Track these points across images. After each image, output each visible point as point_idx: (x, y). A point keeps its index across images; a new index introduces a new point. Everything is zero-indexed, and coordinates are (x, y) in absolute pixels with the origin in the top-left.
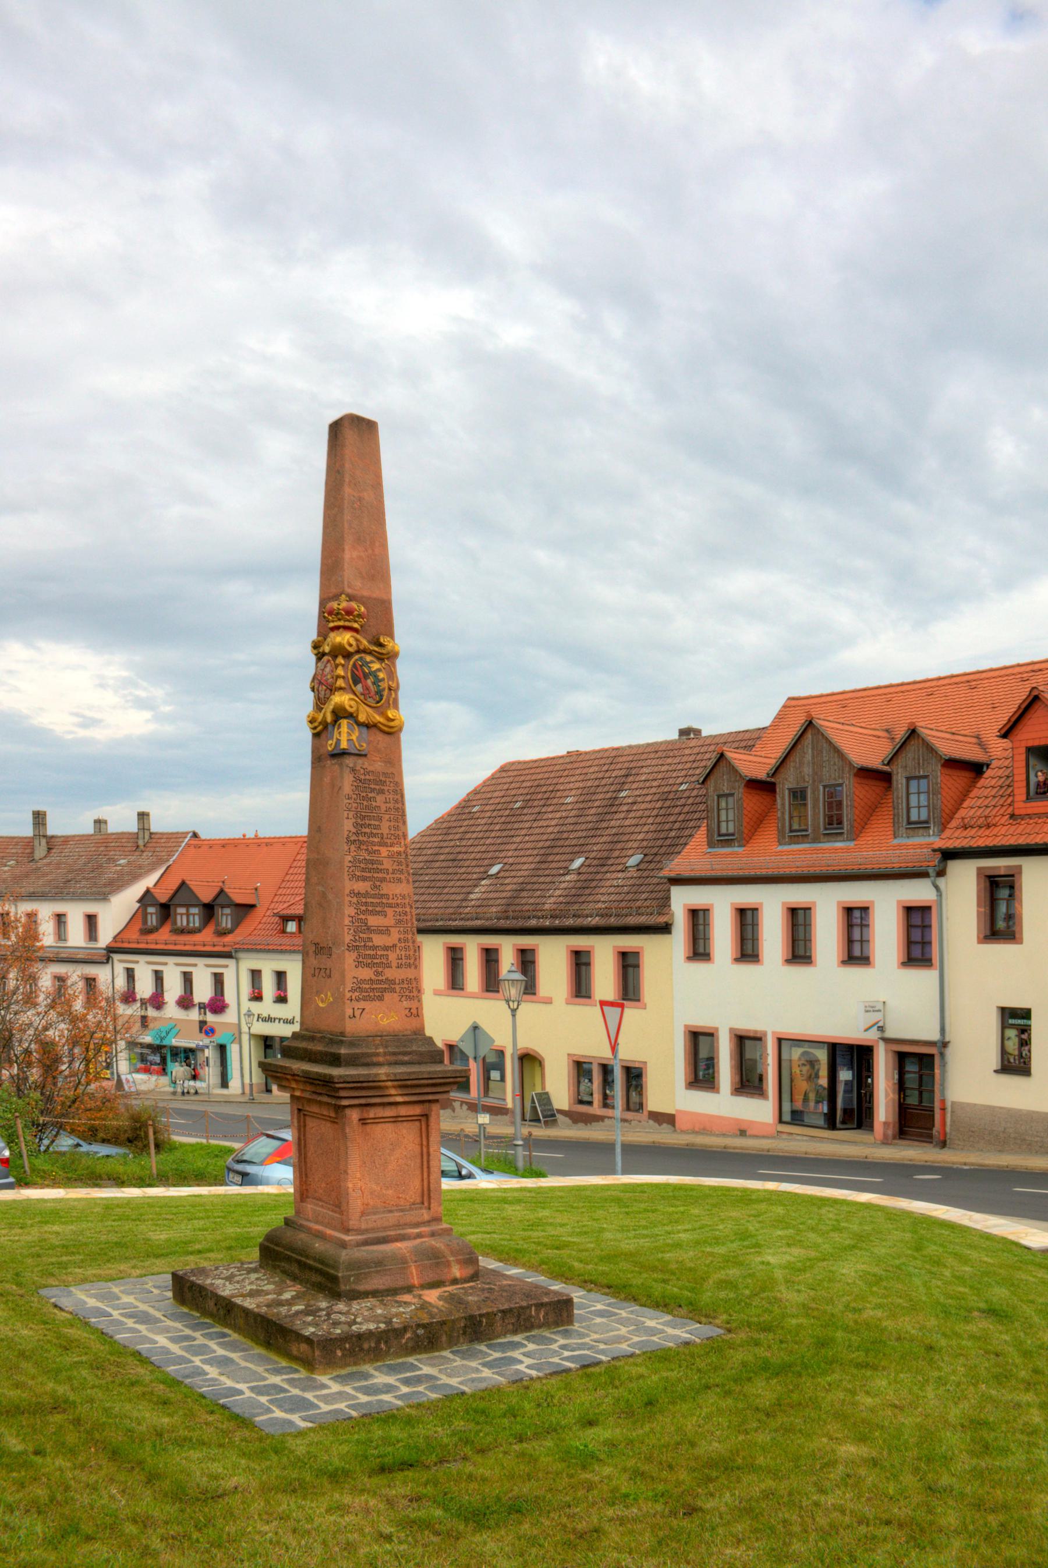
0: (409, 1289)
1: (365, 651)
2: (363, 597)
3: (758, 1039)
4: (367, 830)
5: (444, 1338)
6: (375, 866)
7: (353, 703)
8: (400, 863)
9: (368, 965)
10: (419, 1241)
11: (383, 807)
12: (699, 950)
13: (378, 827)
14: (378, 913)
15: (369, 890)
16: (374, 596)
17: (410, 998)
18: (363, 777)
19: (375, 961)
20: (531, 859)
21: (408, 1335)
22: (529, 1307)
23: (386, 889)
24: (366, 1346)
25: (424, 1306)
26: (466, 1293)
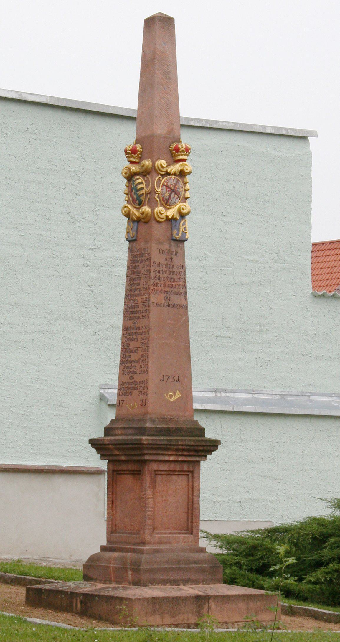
17: (143, 393)
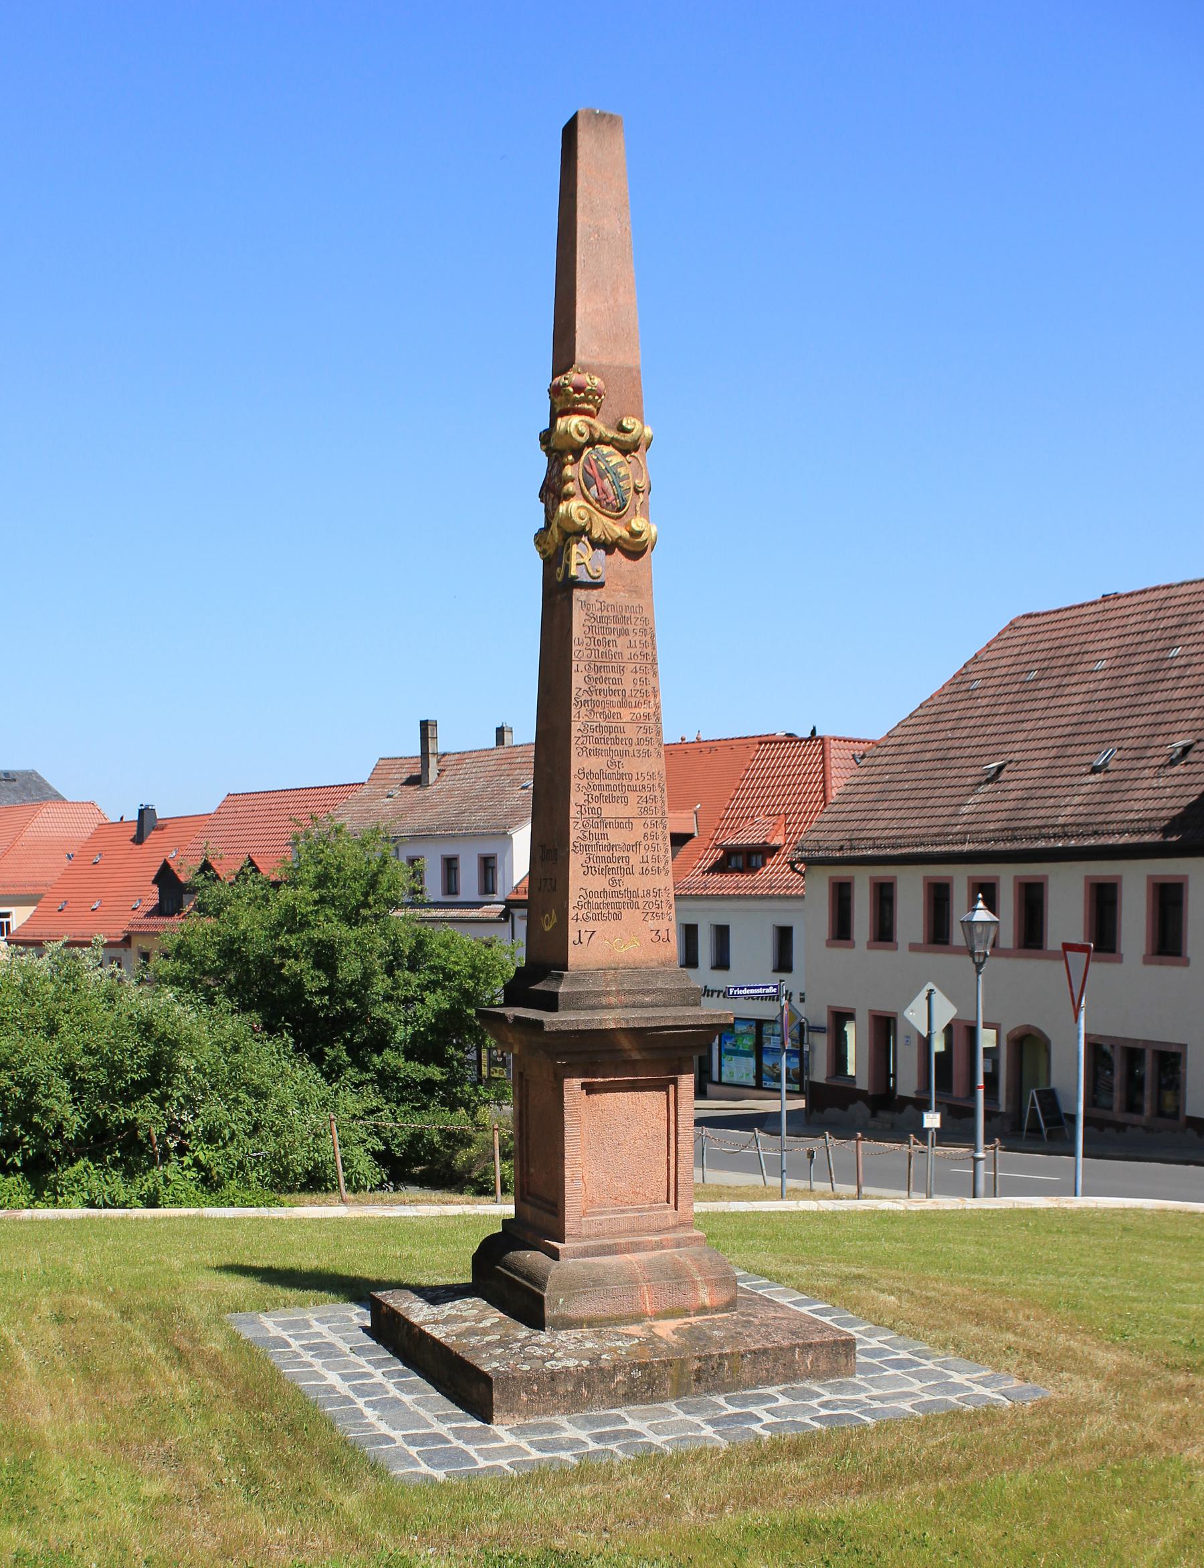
0: (637, 1319)
2: (601, 366)
4: (604, 686)
5: (669, 1384)
6: (613, 735)
7: (582, 512)
9: (600, 871)
10: (657, 1253)
14: (616, 800)
16: (617, 363)
18: (599, 614)
19: (611, 866)
20: (1044, 753)
21: (620, 1377)
22: (792, 1348)
23: (629, 765)
24: (561, 1390)
25: (652, 1340)
26: (711, 1328)
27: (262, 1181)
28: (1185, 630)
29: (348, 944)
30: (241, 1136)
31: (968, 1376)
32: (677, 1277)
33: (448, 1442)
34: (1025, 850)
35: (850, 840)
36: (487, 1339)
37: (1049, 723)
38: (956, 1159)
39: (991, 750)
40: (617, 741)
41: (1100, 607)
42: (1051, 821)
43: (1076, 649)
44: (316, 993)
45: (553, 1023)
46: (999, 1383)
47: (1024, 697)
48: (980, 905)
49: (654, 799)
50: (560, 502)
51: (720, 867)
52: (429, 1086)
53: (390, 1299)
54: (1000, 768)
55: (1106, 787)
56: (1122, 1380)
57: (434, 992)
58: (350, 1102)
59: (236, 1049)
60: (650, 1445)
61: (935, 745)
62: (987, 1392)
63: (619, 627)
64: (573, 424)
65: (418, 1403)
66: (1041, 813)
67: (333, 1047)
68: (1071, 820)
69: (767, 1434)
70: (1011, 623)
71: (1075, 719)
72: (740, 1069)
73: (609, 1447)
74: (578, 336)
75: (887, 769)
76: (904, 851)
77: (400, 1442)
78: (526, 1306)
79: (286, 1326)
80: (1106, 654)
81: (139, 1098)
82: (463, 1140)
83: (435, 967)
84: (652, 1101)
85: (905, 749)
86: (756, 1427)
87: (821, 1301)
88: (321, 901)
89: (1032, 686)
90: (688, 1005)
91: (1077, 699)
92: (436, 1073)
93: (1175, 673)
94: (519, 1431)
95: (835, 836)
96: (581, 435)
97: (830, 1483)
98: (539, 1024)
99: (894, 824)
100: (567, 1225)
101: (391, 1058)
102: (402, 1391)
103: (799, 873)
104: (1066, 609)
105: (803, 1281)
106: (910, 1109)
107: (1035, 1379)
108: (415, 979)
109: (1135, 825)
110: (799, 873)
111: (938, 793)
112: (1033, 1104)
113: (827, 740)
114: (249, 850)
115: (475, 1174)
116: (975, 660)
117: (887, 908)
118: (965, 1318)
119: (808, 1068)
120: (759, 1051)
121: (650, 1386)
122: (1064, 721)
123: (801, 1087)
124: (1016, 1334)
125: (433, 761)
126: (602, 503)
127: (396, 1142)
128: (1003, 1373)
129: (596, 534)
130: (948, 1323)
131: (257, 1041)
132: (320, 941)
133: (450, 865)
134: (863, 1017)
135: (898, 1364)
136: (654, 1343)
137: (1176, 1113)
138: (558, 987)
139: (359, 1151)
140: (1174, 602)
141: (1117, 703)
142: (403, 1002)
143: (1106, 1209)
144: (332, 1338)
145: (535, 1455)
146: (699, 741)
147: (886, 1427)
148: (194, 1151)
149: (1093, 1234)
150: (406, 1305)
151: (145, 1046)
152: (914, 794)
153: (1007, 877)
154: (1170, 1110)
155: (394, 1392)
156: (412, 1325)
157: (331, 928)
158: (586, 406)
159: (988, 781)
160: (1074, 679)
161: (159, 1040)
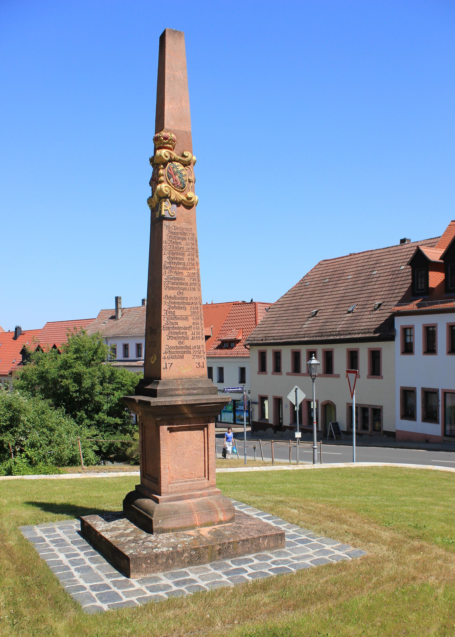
0: (193, 527)
1: (175, 160)
2: (175, 130)
3: (435, 392)
4: (176, 261)
5: (207, 556)
6: (180, 281)
7: (167, 189)
8: (194, 280)
9: (175, 338)
10: (201, 499)
11: (185, 248)
12: (408, 349)
13: (181, 259)
14: (181, 308)
15: (176, 295)
16: (182, 130)
18: (174, 231)
19: (179, 336)
20: (331, 307)
21: (186, 555)
22: (259, 538)
24: (160, 561)
25: (199, 537)
26: (225, 530)
27: (52, 462)
28: (378, 265)
29: (86, 374)
30: (44, 446)
31: (332, 546)
32: (209, 509)
33: (110, 588)
34: (326, 340)
35: (265, 337)
36: (128, 538)
37: (333, 296)
38: (306, 449)
39: (313, 306)
40: (182, 284)
41: (349, 258)
42: (334, 330)
43: (341, 272)
44: (74, 392)
45: (154, 402)
46: (345, 549)
47: (324, 288)
48: (314, 358)
49: (197, 308)
50: (158, 184)
51: (220, 347)
52: (116, 426)
53: (89, 519)
54: (317, 312)
55: (353, 318)
56: (394, 545)
57: (118, 391)
58: (87, 432)
59: (43, 413)
60: (200, 587)
61: (294, 304)
62: (341, 553)
63: (182, 237)
64: (163, 152)
65: (98, 568)
66: (331, 327)
67: (80, 412)
68: (341, 329)
69: (250, 578)
70: (319, 263)
71: (342, 295)
72: (227, 417)
73: (181, 588)
74: (165, 118)
75: (277, 313)
76: (284, 340)
77: (88, 589)
78: (145, 524)
79: (45, 531)
80: (351, 273)
81: (5, 432)
82: (129, 445)
83: (118, 382)
84: (198, 435)
85: (284, 306)
86: (245, 575)
87: (267, 513)
88: (77, 359)
89: (326, 284)
90: (212, 394)
91: (342, 288)
92: (118, 421)
93: (375, 280)
94: (142, 582)
95: (260, 336)
96: (167, 157)
97: (281, 605)
98: (149, 403)
99: (280, 331)
100: (162, 488)
101: (102, 416)
102: (92, 562)
103: (248, 348)
104: (338, 258)
105: (260, 504)
106: (288, 430)
107: (359, 546)
108: (111, 386)
109: (363, 331)
110: (248, 348)
111: (295, 320)
112: (331, 427)
113: (256, 303)
114: (55, 342)
115: (134, 457)
116: (307, 275)
117: (279, 360)
118: (327, 520)
119: (252, 416)
120: (234, 411)
121: (199, 558)
122: (338, 296)
123: (249, 423)
124: (348, 525)
125: (120, 311)
126: (175, 185)
127: (104, 447)
128: (346, 544)
129: (173, 198)
130: (320, 521)
131: (51, 410)
132: (76, 372)
133: (126, 347)
134: (271, 399)
135: (302, 541)
136: (200, 538)
137: (380, 429)
138: (157, 387)
139: (90, 450)
140: (373, 256)
141: (356, 290)
142: (106, 395)
143: (365, 467)
144: (64, 537)
145: (149, 594)
146: (212, 304)
147: (302, 573)
148: (26, 452)
149: (363, 477)
150: (94, 523)
151: (8, 412)
152: (287, 321)
153: (320, 349)
154: (377, 429)
155: (88, 563)
156: (97, 532)
157: (80, 368)
158: (169, 146)
159: (312, 316)
160: (341, 282)
161: (14, 410)
